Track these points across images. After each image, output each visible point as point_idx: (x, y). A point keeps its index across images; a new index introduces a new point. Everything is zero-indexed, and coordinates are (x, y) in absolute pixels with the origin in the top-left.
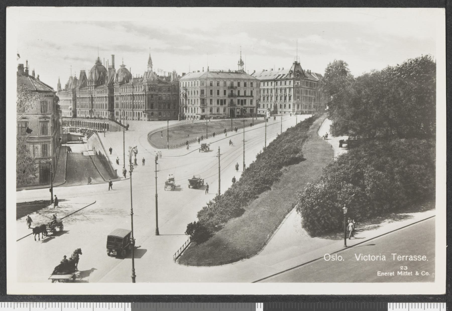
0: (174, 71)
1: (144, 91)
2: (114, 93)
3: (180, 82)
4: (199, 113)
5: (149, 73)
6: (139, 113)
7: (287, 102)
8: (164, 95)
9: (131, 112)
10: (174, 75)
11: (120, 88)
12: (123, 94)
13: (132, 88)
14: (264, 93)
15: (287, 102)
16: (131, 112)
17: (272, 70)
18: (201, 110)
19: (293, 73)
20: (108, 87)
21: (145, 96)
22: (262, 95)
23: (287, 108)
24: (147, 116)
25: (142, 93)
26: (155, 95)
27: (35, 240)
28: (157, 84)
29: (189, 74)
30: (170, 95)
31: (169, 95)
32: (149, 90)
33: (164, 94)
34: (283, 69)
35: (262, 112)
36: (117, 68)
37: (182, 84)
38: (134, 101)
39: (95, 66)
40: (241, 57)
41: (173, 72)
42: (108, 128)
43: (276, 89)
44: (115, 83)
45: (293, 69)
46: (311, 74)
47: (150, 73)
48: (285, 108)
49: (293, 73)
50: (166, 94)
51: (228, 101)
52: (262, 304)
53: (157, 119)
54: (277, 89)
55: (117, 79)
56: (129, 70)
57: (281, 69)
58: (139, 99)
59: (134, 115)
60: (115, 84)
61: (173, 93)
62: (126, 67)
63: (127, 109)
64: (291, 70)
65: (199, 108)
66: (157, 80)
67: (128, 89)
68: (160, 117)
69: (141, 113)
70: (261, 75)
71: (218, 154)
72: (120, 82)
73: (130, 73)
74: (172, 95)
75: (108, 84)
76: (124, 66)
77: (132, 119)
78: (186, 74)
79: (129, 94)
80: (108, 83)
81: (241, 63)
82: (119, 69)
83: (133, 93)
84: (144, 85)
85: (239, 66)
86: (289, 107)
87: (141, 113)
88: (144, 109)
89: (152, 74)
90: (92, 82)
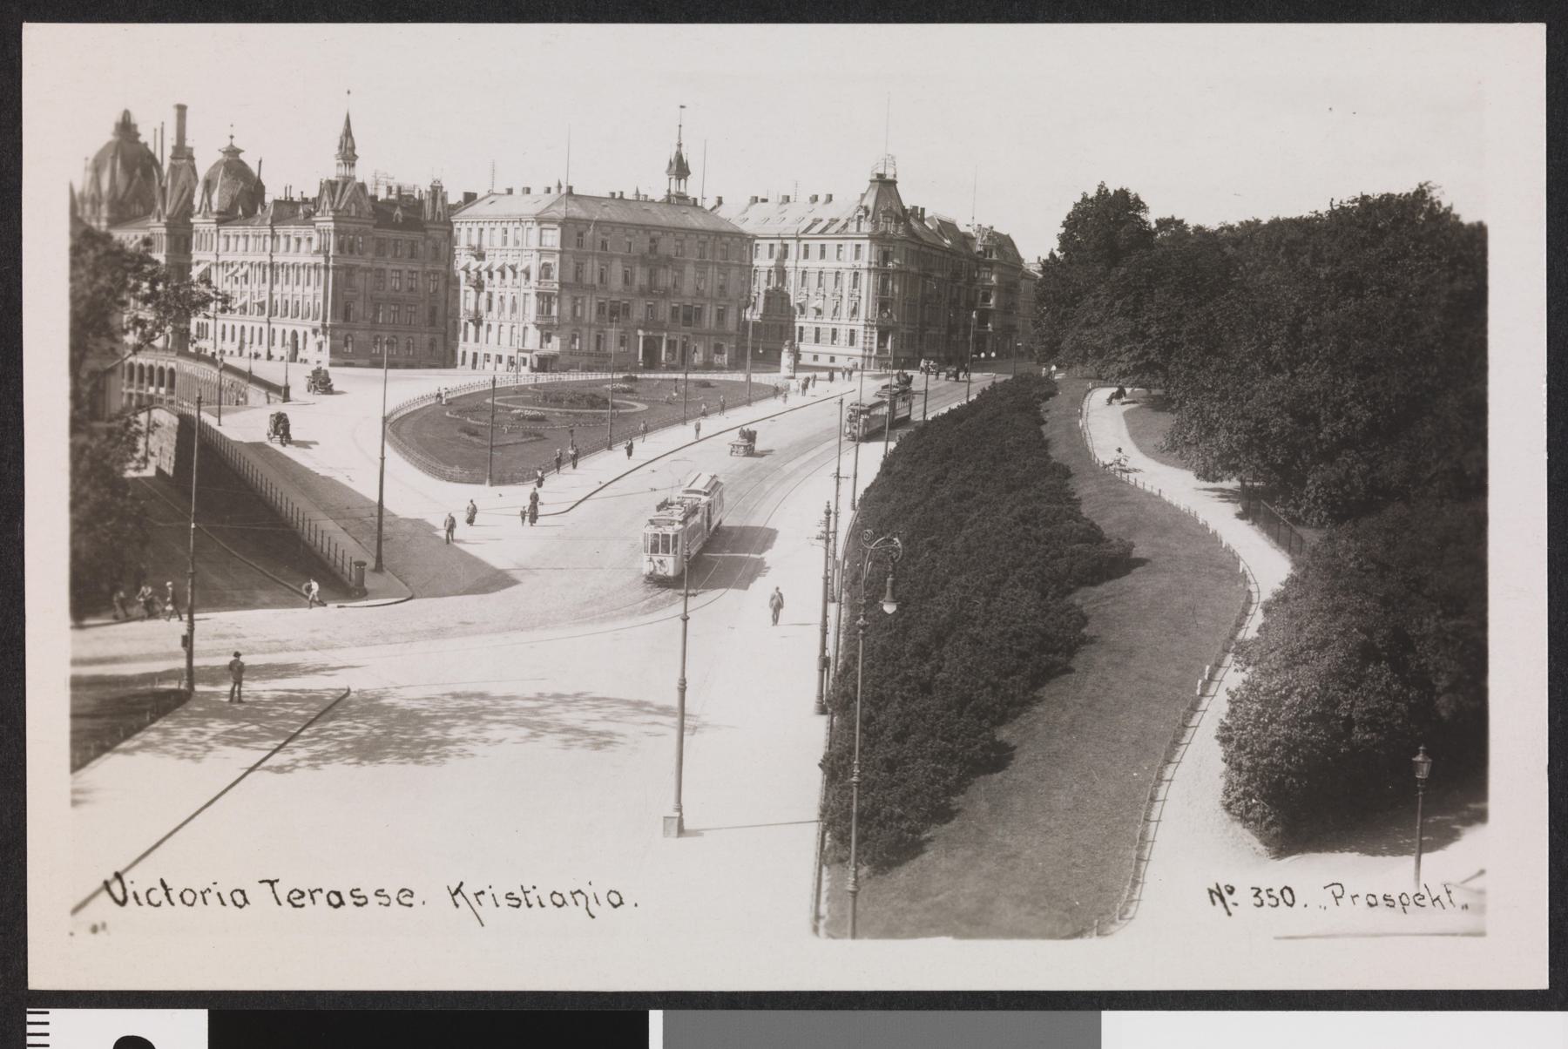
0: (436, 185)
1: (318, 252)
2: (193, 251)
3: (457, 226)
4: (529, 346)
5: (340, 187)
6: (295, 334)
7: (841, 321)
8: (396, 271)
9: (261, 329)
10: (434, 199)
11: (218, 237)
12: (230, 259)
13: (268, 239)
14: (855, 286)
15: (841, 321)
16: (261, 329)
17: (787, 199)
18: (538, 333)
19: (869, 217)
20: (167, 225)
21: (322, 272)
22: (846, 295)
23: (843, 343)
24: (327, 347)
25: (311, 261)
26: (360, 271)
27: (411, 905)
28: (370, 227)
29: (492, 198)
30: (416, 272)
31: (412, 272)
32: (340, 247)
33: (392, 267)
34: (830, 198)
35: (811, 356)
36: (206, 159)
37: (464, 233)
38: (277, 288)
39: (109, 144)
40: (680, 145)
41: (432, 186)
42: (172, 385)
43: (800, 270)
44: (199, 212)
45: (870, 202)
46: (926, 223)
47: (345, 185)
48: (832, 343)
49: (869, 217)
50: (401, 268)
51: (639, 311)
52: (30, 1018)
53: (367, 362)
54: (804, 272)
55: (206, 201)
56: (254, 169)
57: (822, 198)
58: (287, 283)
59: (271, 342)
60: (196, 220)
61: (429, 268)
62: (242, 156)
63: (247, 316)
64: (864, 204)
65: (532, 328)
66: (369, 214)
67: (251, 240)
68: (376, 355)
69: (305, 333)
70: (746, 216)
71: (824, 529)
72: (219, 213)
73: (259, 181)
74: (423, 272)
75: (169, 218)
76: (238, 152)
77: (264, 355)
78: (478, 198)
79: (257, 260)
80: (168, 212)
81: (680, 169)
82: (216, 165)
83: (271, 257)
84: (319, 231)
85: (673, 180)
86: (848, 339)
87: (305, 333)
88: (318, 323)
89: (355, 189)
90: (100, 205)
